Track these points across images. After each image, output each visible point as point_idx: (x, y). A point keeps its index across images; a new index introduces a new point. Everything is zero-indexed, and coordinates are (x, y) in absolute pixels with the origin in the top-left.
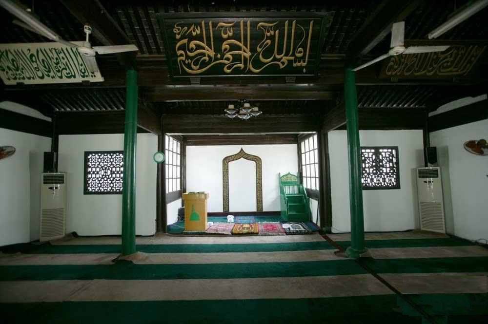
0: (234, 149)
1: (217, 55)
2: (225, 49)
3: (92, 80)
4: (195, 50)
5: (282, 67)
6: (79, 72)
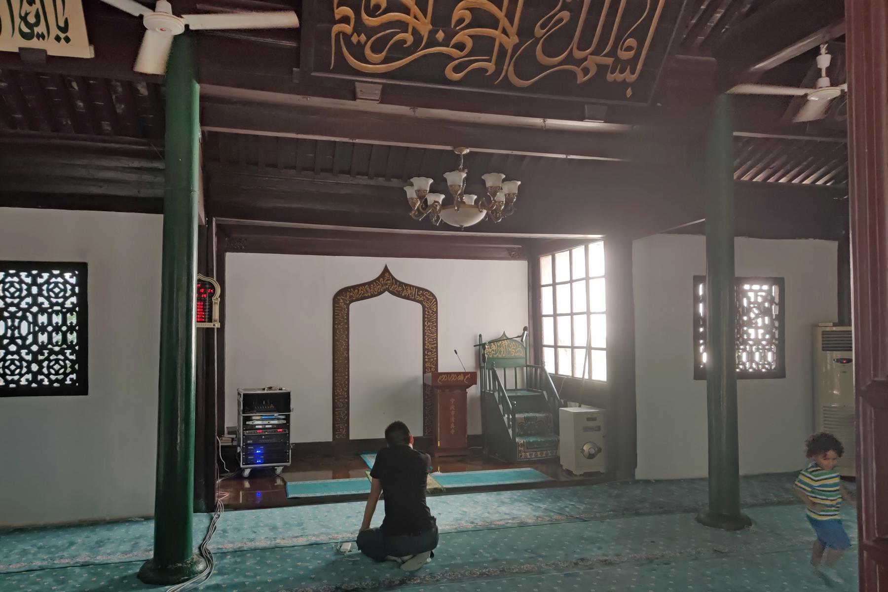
0: (363, 268)
1: (438, 31)
2: (461, 21)
3: (55, 49)
4: (386, 11)
5: (581, 79)
6: (17, 20)
